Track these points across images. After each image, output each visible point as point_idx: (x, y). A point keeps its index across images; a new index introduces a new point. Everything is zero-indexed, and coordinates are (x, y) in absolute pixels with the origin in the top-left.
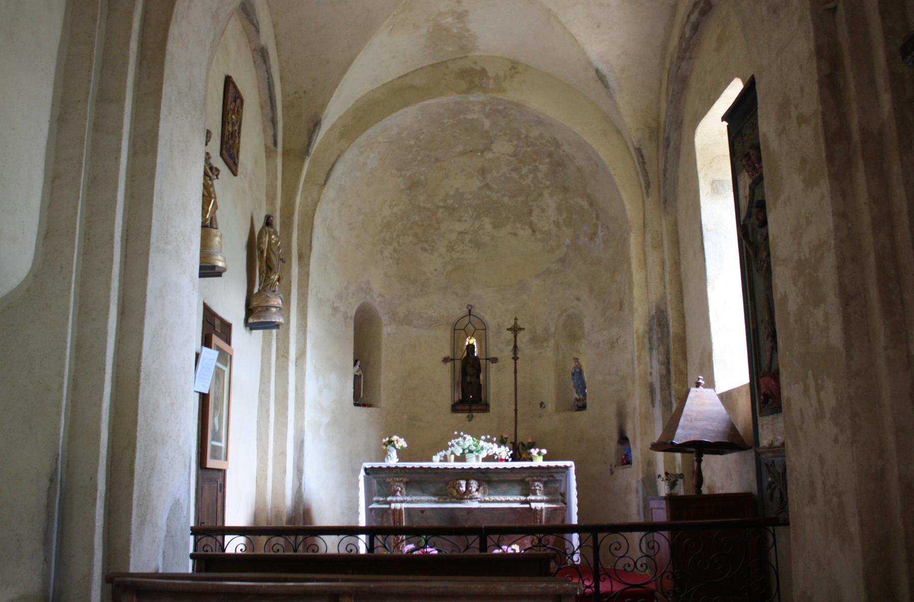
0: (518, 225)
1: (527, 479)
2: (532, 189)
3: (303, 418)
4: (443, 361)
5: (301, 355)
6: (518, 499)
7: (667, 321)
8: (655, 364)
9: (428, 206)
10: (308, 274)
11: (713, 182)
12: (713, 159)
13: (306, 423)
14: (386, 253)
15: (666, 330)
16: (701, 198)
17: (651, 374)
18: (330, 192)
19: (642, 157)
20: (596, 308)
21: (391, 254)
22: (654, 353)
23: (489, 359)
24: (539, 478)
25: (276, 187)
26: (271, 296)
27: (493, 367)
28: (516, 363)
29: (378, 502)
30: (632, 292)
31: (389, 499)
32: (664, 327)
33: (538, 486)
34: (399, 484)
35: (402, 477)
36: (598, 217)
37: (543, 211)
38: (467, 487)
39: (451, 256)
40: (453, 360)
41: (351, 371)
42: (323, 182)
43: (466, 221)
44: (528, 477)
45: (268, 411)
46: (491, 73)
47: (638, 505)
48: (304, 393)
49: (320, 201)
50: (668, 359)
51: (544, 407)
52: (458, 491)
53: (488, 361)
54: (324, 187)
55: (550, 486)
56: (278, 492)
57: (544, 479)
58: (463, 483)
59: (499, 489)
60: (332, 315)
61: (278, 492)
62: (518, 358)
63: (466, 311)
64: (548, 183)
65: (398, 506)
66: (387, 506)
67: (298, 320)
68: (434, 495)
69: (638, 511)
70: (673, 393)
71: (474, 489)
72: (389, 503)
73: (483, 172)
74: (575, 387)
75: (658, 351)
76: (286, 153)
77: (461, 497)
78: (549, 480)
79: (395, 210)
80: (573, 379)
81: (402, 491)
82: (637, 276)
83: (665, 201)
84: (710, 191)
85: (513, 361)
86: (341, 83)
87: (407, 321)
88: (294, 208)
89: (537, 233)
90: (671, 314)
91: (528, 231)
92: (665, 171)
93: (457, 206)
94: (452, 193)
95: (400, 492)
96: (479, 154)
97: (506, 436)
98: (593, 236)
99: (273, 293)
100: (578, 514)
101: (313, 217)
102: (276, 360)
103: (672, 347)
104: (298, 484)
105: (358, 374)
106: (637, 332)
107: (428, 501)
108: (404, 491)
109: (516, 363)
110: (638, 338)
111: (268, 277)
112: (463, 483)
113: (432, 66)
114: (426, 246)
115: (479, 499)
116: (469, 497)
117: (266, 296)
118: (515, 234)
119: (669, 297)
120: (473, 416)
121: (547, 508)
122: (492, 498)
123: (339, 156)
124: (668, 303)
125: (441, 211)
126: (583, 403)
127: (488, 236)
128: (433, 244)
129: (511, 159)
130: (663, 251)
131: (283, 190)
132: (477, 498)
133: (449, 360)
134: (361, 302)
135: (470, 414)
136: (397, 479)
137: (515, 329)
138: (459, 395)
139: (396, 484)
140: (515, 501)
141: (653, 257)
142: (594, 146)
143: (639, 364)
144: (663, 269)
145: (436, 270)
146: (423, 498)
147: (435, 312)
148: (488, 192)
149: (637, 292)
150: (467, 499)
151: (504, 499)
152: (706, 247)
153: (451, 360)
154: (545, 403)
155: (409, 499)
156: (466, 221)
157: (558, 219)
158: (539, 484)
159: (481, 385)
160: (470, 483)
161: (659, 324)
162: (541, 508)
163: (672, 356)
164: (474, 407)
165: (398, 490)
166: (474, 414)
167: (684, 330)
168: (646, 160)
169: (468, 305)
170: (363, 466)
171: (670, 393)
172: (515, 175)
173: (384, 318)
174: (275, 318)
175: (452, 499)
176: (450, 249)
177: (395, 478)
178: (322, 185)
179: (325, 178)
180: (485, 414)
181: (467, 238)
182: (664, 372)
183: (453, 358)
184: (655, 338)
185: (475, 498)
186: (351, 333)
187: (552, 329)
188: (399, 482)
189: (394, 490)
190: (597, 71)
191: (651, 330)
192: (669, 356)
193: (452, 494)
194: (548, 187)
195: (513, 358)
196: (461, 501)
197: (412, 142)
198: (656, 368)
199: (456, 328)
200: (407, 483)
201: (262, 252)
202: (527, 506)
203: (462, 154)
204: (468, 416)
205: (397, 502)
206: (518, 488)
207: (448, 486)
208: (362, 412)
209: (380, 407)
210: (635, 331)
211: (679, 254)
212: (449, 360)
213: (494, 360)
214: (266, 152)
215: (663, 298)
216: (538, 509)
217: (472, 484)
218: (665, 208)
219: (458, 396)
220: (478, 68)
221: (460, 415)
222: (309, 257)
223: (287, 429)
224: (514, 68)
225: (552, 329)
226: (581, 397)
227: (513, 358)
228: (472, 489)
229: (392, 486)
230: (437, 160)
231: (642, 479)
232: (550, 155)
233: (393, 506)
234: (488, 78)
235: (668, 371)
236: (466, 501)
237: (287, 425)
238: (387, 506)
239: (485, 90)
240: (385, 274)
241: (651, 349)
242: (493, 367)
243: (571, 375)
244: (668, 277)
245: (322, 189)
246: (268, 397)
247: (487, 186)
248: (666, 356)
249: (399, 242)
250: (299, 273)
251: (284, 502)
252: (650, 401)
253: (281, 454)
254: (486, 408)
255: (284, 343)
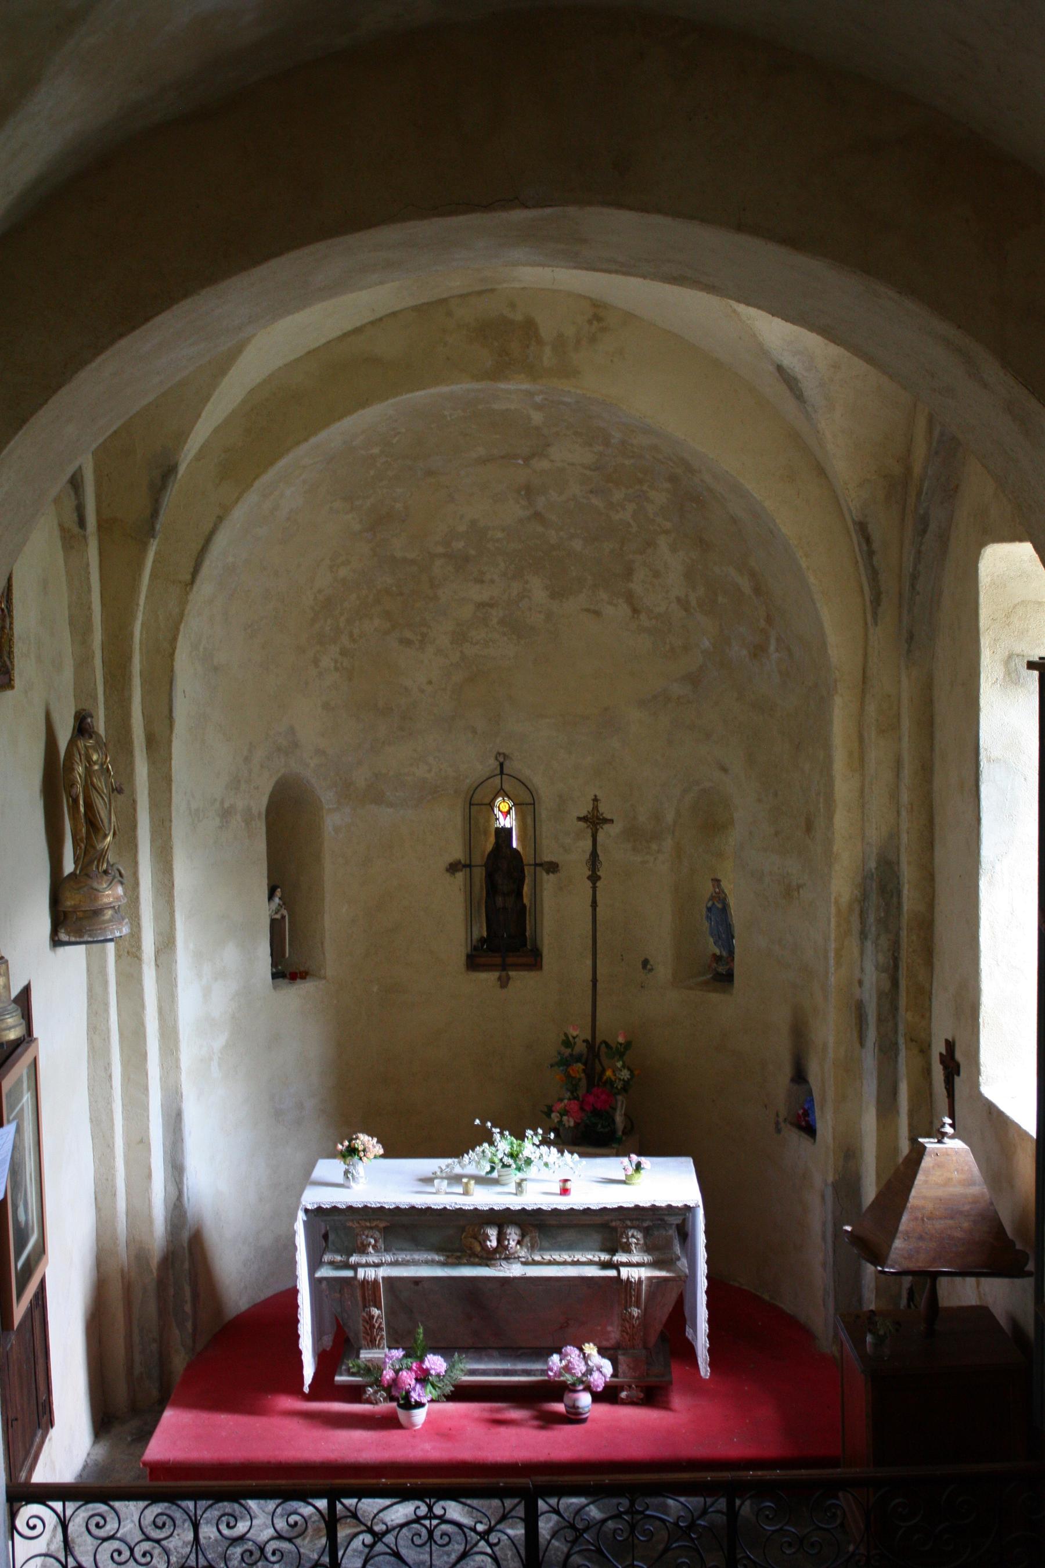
0: (603, 595)
1: (614, 1224)
2: (634, 529)
3: (178, 1067)
4: (447, 870)
5: (166, 944)
6: (596, 1259)
7: (899, 883)
8: (869, 967)
9: (411, 556)
10: (168, 779)
11: (1010, 657)
12: (1015, 607)
13: (184, 1077)
14: (326, 662)
15: (895, 900)
16: (982, 691)
17: (860, 983)
18: (205, 588)
19: (868, 540)
20: (760, 800)
21: (336, 661)
22: (869, 945)
23: (541, 865)
24: (636, 1223)
25: (90, 608)
26: (100, 887)
27: (549, 881)
28: (594, 888)
29: (333, 1264)
30: (830, 818)
31: (353, 1259)
32: (892, 896)
33: (633, 1236)
34: (371, 1233)
35: (377, 1219)
36: (769, 619)
37: (657, 574)
38: (500, 1240)
39: (461, 652)
40: (469, 866)
41: (263, 911)
42: (188, 577)
43: (492, 581)
44: (615, 1220)
45: (108, 1067)
46: (547, 330)
47: (824, 1224)
48: (176, 1021)
49: (185, 618)
50: (896, 960)
51: (651, 970)
52: (484, 1248)
53: (538, 868)
54: (191, 589)
55: (656, 1233)
56: (138, 1214)
57: (645, 1224)
58: (492, 1233)
59: (559, 1239)
60: (221, 828)
61: (138, 1214)
62: (599, 878)
63: (492, 763)
64: (668, 525)
65: (371, 1274)
66: (349, 1273)
67: (154, 874)
68: (438, 1250)
69: (824, 1233)
70: (901, 1028)
71: (513, 1244)
72: (354, 1267)
73: (528, 492)
74: (712, 934)
75: (877, 945)
76: (104, 526)
77: (488, 1258)
78: (653, 1224)
79: (343, 572)
80: (708, 918)
81: (378, 1245)
82: (843, 788)
83: (911, 637)
84: (1001, 677)
85: (589, 884)
86: (216, 393)
87: (374, 795)
88: (130, 647)
89: (643, 616)
90: (908, 872)
91: (623, 609)
92: (914, 577)
93: (473, 552)
94: (462, 528)
95: (374, 1247)
96: (520, 462)
97: (575, 1034)
98: (759, 651)
99: (105, 878)
100: (707, 1292)
101: (172, 655)
102: (116, 962)
103: (905, 940)
104: (177, 1193)
105: (278, 916)
106: (836, 902)
107: (427, 1263)
108: (381, 1244)
109: (594, 888)
110: (839, 912)
111: (90, 845)
112: (492, 1233)
113: (416, 309)
114: (408, 634)
115: (523, 1260)
116: (503, 1256)
117: (92, 888)
118: (597, 613)
119: (904, 838)
120: (508, 978)
121: (650, 1279)
122: (547, 1257)
123: (220, 519)
124: (903, 850)
125: (438, 563)
126: (728, 967)
127: (540, 612)
128: (424, 630)
129: (588, 472)
130: (900, 739)
131: (103, 605)
132: (519, 1257)
133: (460, 866)
134: (280, 775)
135: (504, 973)
136: (368, 1224)
137: (594, 821)
138: (481, 927)
139: (366, 1232)
140: (590, 1263)
141: (877, 753)
142: (767, 504)
143: (838, 964)
144: (898, 776)
145: (430, 682)
146: (417, 1256)
147: (430, 771)
148: (540, 529)
149: (841, 821)
150: (500, 1259)
151: (569, 1260)
152: (983, 796)
153: (465, 866)
154: (651, 962)
155: (388, 1258)
156: (492, 581)
157: (687, 596)
158: (635, 1234)
159: (524, 906)
160: (505, 1234)
161: (883, 890)
162: (640, 1278)
163: (904, 954)
164: (510, 960)
165: (370, 1243)
166: (511, 973)
167: (931, 906)
168: (876, 546)
169: (499, 754)
170: (301, 1207)
171: (896, 1025)
172: (597, 501)
173: (327, 797)
174: (112, 932)
175: (472, 1259)
176: (460, 637)
177: (363, 1223)
178: (187, 585)
179: (192, 570)
180: (533, 974)
181: (496, 614)
182: (887, 986)
183: (468, 862)
184: (871, 919)
185: (515, 1258)
186: (261, 846)
187: (670, 817)
188: (371, 1228)
189: (362, 1243)
190: (780, 368)
191: (865, 897)
192: (899, 953)
193: (471, 1249)
194: (667, 532)
195: (589, 878)
196: (489, 1262)
197: (376, 450)
198: (871, 977)
199: (474, 801)
200: (385, 1228)
201: (76, 801)
202: (612, 1273)
203: (483, 461)
204: (500, 979)
205: (367, 1265)
206: (597, 1238)
207: (464, 1234)
208: (295, 994)
209: (325, 978)
210: (833, 900)
211: (932, 749)
212: (460, 866)
213: (552, 867)
214: (63, 539)
215: (894, 836)
216: (633, 1280)
217: (510, 1234)
218: (909, 651)
219: (481, 930)
220: (519, 317)
221: (483, 975)
222: (170, 741)
223: (147, 1096)
224: (597, 318)
225: (670, 817)
226: (724, 954)
227: (589, 878)
228: (509, 1244)
229: (357, 1235)
230: (430, 473)
231: (833, 1183)
232: (673, 479)
233: (361, 1273)
234: (540, 342)
235: (895, 983)
236: (498, 1262)
237: (147, 1089)
238: (349, 1273)
239: (532, 371)
240: (326, 706)
241: (863, 935)
242: (549, 881)
243: (704, 910)
244: (905, 797)
245: (187, 594)
246: (107, 1039)
247: (538, 516)
248: (893, 955)
249: (351, 635)
250: (150, 775)
251: (152, 1232)
252: (855, 1035)
253: (139, 1143)
254: (533, 960)
255: (131, 951)
